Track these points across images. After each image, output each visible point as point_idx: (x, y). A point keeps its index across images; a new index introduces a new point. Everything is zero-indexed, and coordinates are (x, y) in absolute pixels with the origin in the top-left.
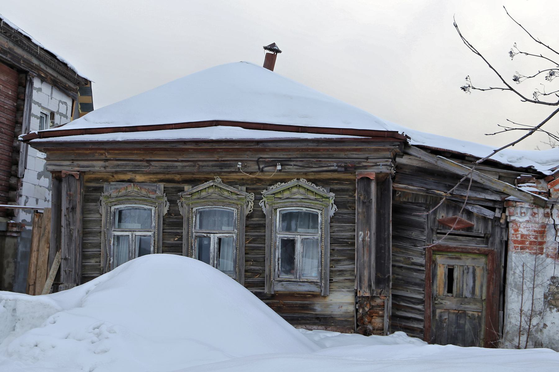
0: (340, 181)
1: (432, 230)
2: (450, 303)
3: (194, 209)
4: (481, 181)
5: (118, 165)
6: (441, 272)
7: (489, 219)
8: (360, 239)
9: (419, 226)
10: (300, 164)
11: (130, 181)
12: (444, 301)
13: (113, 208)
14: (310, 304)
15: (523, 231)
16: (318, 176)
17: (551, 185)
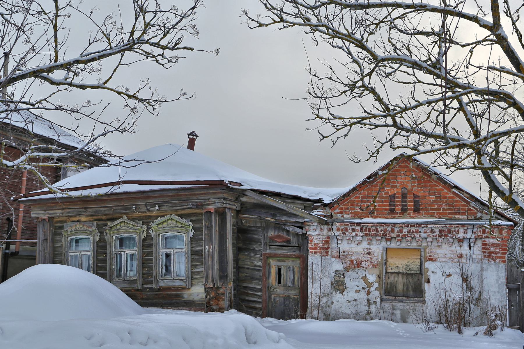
0: (196, 214)
1: (266, 243)
3: (114, 237)
4: (288, 210)
5: (69, 212)
6: (274, 271)
8: (207, 251)
9: (259, 242)
10: (170, 205)
11: (78, 221)
13: (69, 238)
14: (181, 294)
15: (315, 241)
16: (183, 212)
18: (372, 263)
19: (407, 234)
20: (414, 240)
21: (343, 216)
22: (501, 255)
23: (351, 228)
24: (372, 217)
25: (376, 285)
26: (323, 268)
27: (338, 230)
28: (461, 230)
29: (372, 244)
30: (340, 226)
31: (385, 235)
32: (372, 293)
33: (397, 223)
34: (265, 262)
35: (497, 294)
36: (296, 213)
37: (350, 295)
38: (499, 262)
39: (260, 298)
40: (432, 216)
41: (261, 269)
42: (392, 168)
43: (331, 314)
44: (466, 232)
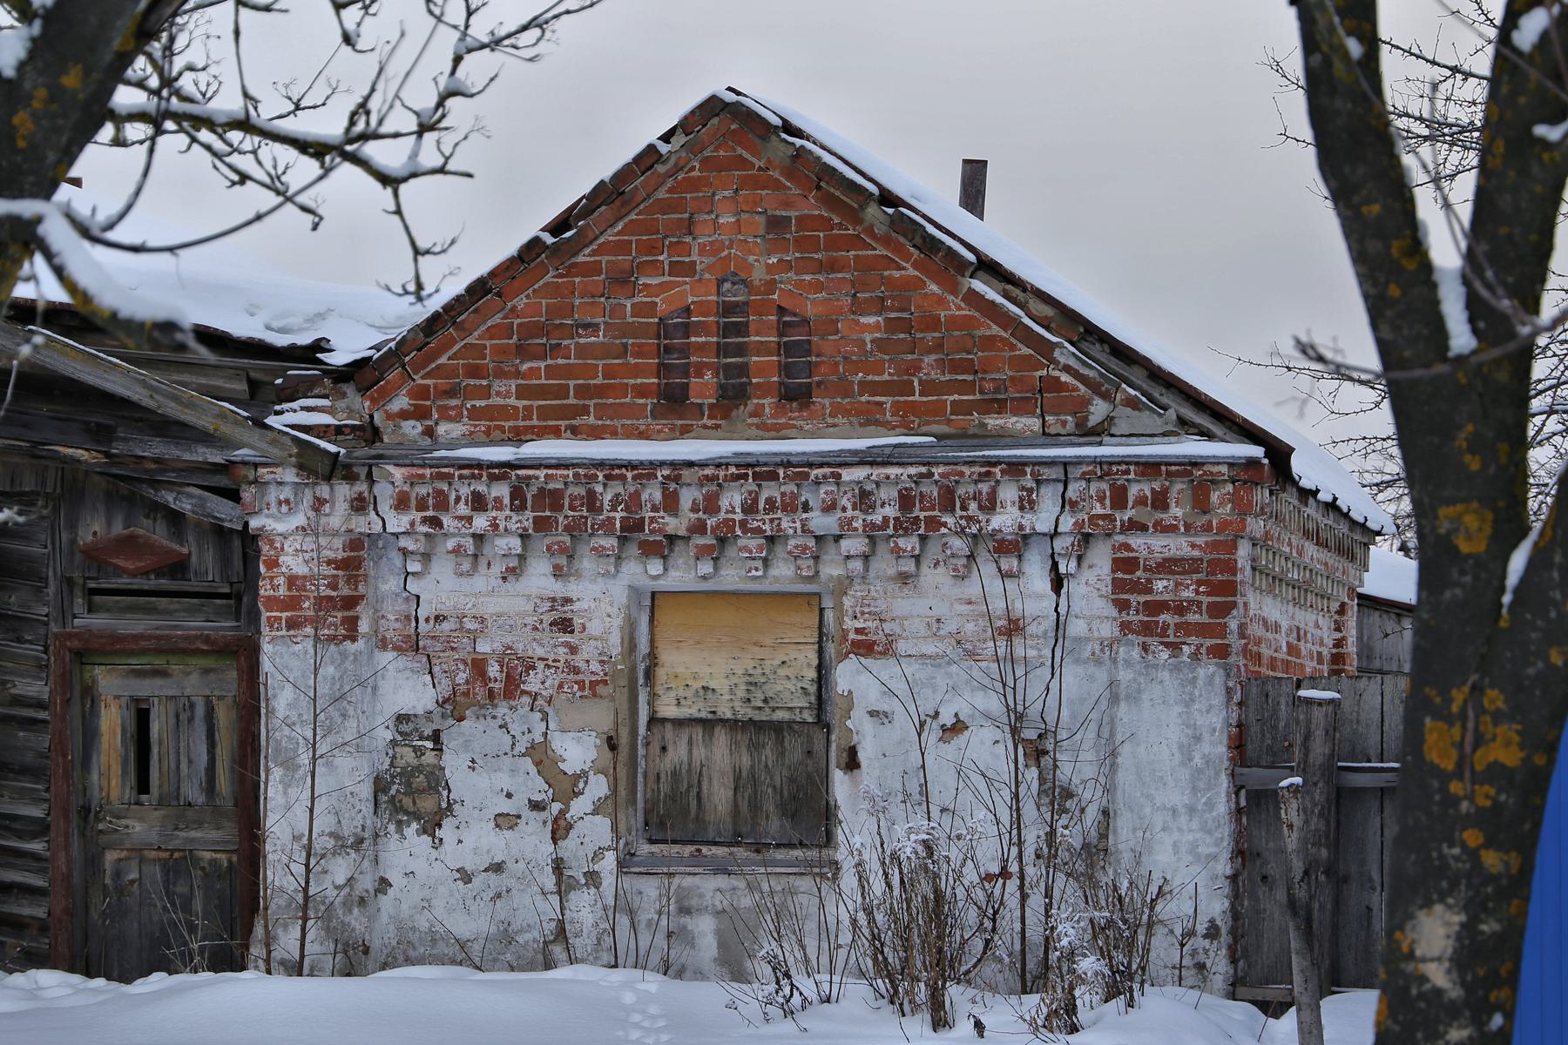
1: (70, 582)
2: (141, 827)
4: (150, 404)
6: (112, 722)
7: (231, 530)
12: (124, 822)
15: (293, 563)
17: (374, 401)
18: (576, 671)
19: (739, 516)
20: (779, 550)
21: (429, 432)
22: (1205, 619)
23: (465, 491)
24: (575, 432)
25: (598, 787)
26: (325, 711)
27: (401, 503)
28: (1009, 493)
29: (578, 575)
30: (412, 481)
31: (632, 527)
32: (579, 828)
33: (690, 464)
34: (65, 680)
35: (1183, 819)
36: (188, 417)
37: (469, 841)
38: (1195, 656)
39: (41, 871)
40: (868, 423)
41: (43, 715)
42: (669, 174)
43: (375, 944)
44: (1032, 503)
